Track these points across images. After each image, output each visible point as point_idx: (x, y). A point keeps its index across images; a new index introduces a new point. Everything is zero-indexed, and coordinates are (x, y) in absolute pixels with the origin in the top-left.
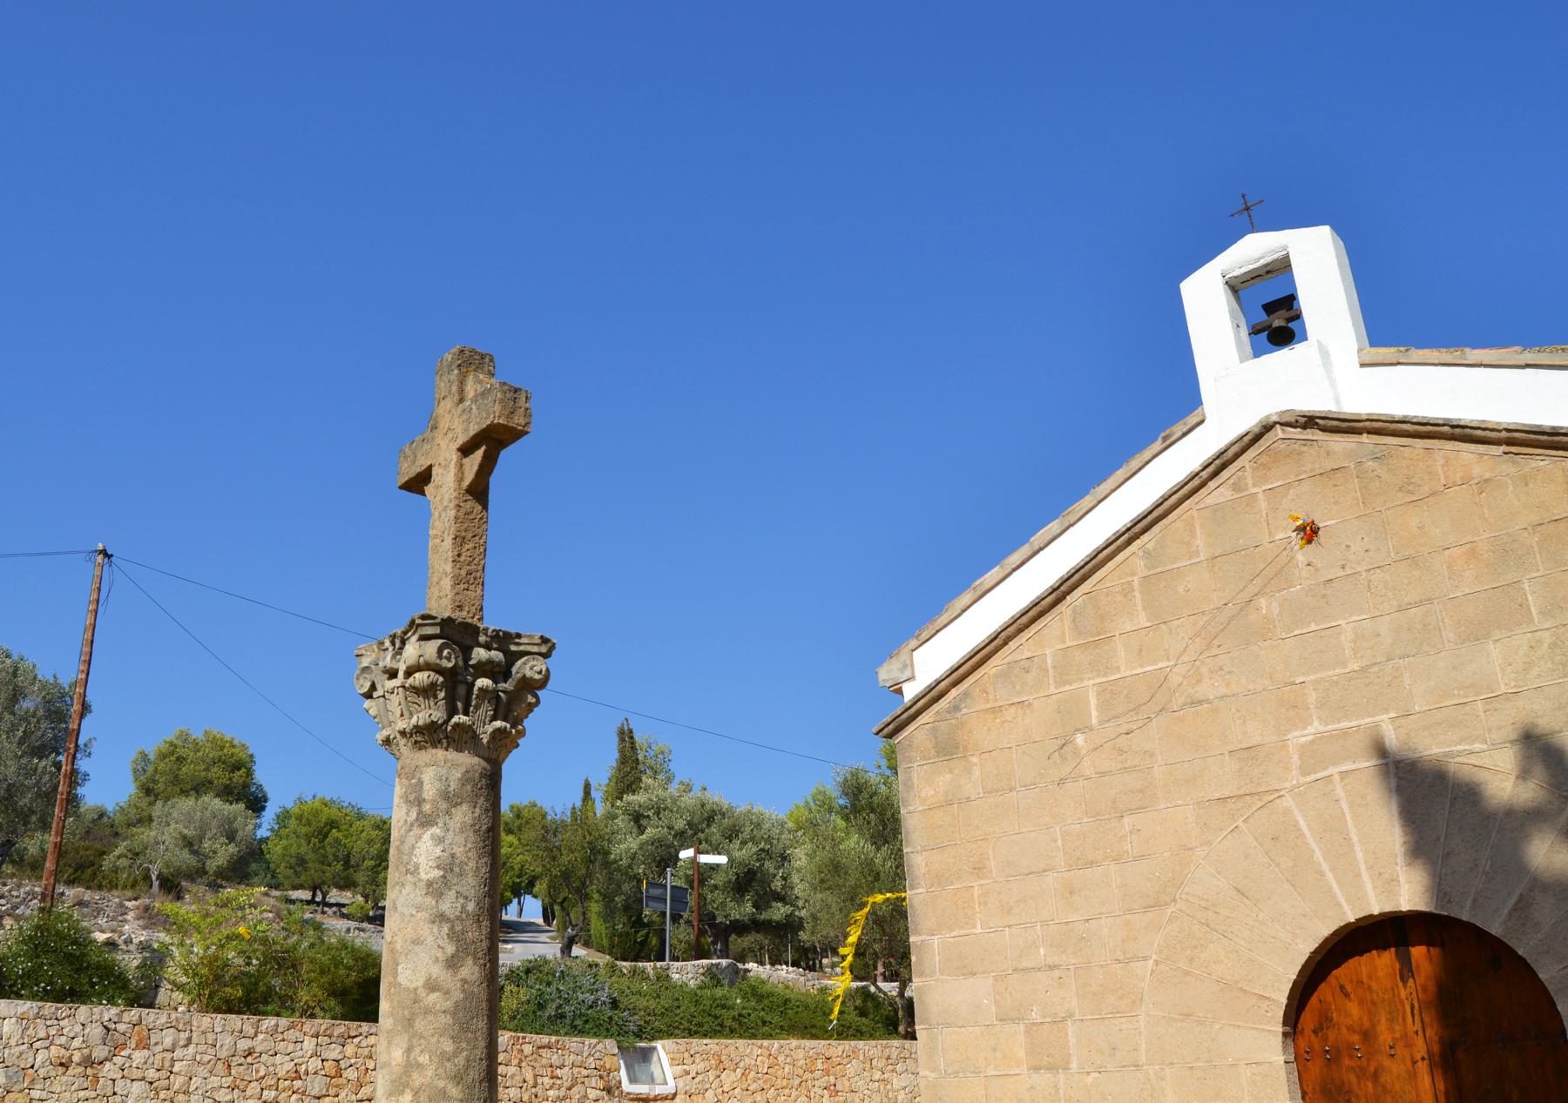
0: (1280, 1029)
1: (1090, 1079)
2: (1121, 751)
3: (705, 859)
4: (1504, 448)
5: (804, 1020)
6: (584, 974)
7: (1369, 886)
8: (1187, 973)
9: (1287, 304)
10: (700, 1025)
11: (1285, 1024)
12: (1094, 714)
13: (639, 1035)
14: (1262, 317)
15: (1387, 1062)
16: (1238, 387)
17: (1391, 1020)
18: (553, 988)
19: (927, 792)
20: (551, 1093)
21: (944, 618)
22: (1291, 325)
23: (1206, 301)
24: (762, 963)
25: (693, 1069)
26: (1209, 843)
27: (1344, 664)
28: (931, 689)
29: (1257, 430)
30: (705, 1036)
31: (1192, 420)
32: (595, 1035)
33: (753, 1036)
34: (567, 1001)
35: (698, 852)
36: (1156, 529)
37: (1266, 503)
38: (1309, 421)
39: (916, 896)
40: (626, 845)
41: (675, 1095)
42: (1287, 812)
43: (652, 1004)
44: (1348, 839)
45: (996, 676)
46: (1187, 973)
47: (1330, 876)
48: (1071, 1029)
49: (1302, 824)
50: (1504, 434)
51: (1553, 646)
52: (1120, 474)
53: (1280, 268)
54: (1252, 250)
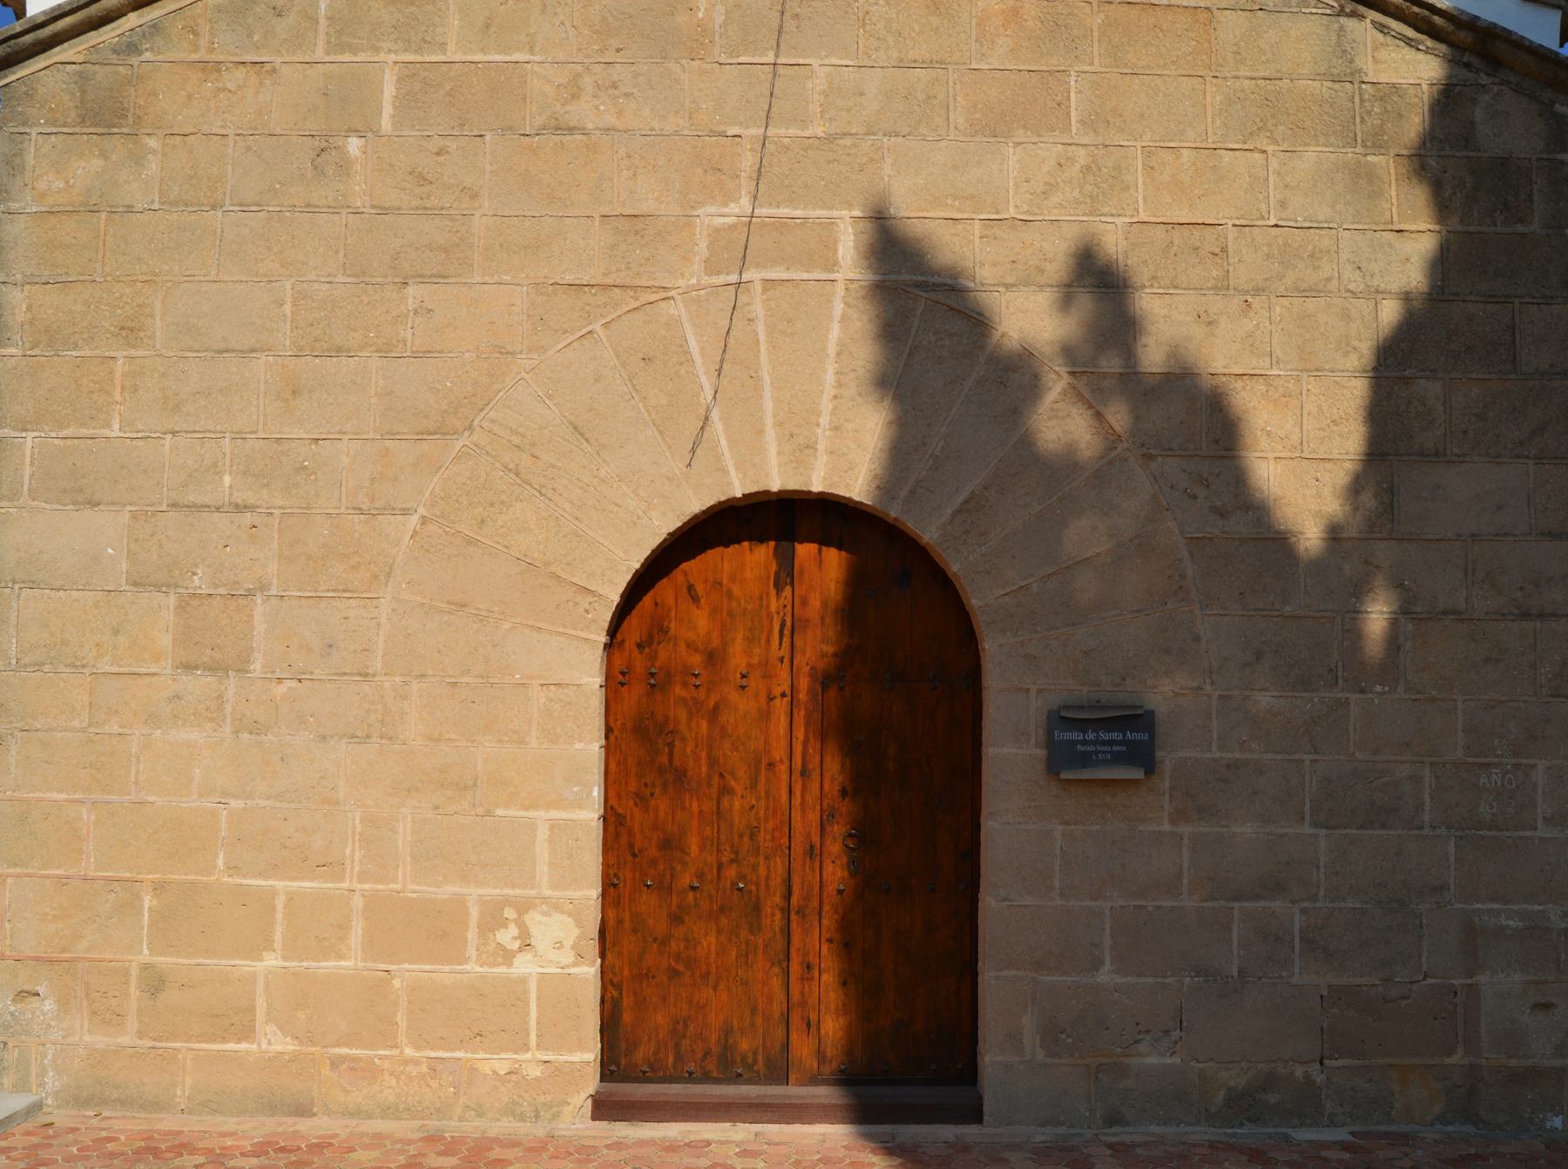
2: (423, 180)
7: (772, 449)
8: (471, 542)
12: (388, 109)
15: (734, 696)
17: (751, 639)
19: (51, 182)
26: (543, 349)
27: (804, 123)
44: (755, 379)
48: (260, 609)
51: (1087, 169)
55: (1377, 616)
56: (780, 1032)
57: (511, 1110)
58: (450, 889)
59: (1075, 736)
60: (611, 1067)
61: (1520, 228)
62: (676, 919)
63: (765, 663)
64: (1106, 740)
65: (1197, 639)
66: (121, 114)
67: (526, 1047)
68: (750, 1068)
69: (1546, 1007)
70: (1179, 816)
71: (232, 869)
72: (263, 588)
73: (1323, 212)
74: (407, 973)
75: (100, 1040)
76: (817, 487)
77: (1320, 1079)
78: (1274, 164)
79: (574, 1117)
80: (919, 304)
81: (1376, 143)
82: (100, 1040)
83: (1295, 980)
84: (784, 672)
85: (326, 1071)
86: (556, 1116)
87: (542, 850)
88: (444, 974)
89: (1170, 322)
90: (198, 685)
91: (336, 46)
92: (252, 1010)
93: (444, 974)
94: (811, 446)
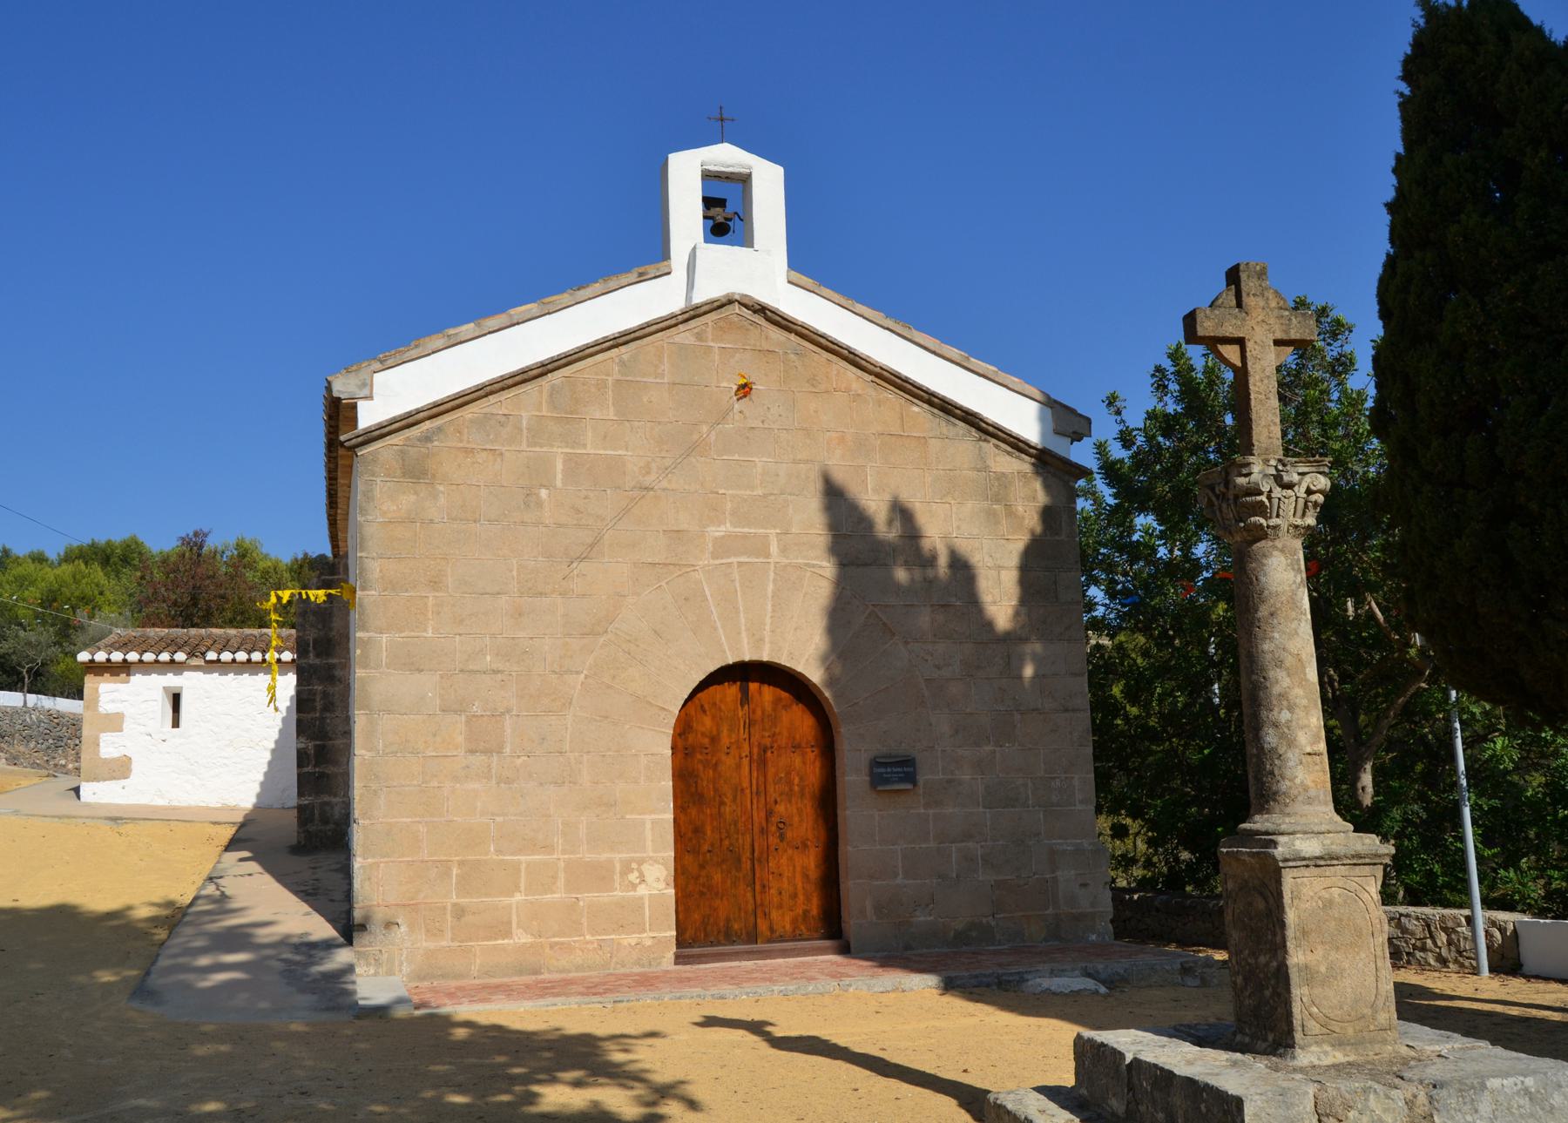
2: (578, 511)
4: (872, 378)
8: (609, 687)
12: (559, 476)
15: (724, 757)
17: (731, 730)
21: (414, 353)
23: (685, 174)
37: (725, 358)
38: (762, 310)
45: (471, 421)
48: (508, 722)
54: (726, 156)
58: (605, 856)
59: (882, 770)
60: (680, 943)
62: (702, 867)
63: (737, 741)
64: (895, 772)
66: (424, 473)
67: (644, 931)
69: (1084, 885)
70: (927, 806)
71: (499, 852)
72: (509, 711)
74: (587, 897)
75: (431, 945)
76: (765, 659)
77: (993, 924)
84: (746, 746)
85: (547, 950)
87: (648, 834)
88: (604, 897)
90: (478, 760)
92: (510, 923)
93: (604, 897)
94: (762, 639)
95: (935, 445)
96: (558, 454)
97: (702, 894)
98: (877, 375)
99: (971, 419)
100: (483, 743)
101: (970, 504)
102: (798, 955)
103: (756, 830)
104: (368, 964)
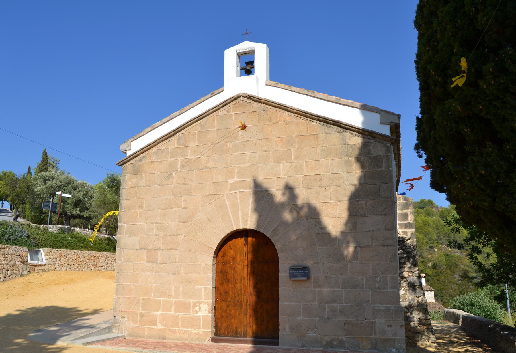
0: (213, 256)
1: (162, 266)
2: (185, 179)
3: (64, 195)
4: (295, 114)
5: (83, 244)
6: (19, 227)
7: (241, 221)
8: (192, 240)
9: (251, 63)
10: (56, 244)
11: (214, 254)
13: (35, 246)
14: (245, 65)
15: (237, 266)
16: (234, 84)
18: (8, 230)
19: (129, 183)
20: (3, 262)
21: (142, 134)
22: (252, 69)
23: (230, 56)
24: (81, 228)
25: (52, 257)
26: (203, 206)
27: (245, 163)
28: (135, 153)
29: (236, 97)
30: (57, 248)
31: (220, 90)
32: (21, 245)
33: (73, 249)
34: (12, 235)
35: (62, 193)
36: (205, 119)
37: (235, 116)
38: (250, 97)
39: (122, 213)
40: (39, 188)
41: (45, 265)
42: (224, 200)
43: (41, 237)
44: (238, 209)
45: (154, 153)
46: (192, 240)
47: (232, 218)
49: (227, 204)
50: (295, 111)
51: (295, 167)
52: (198, 101)
53: (251, 53)
54: (245, 46)
55: (351, 249)
56: (246, 328)
57: (197, 340)
58: (188, 300)
59: (294, 272)
61: (380, 169)
62: (228, 307)
63: (243, 260)
64: (301, 272)
65: (317, 253)
68: (240, 335)
69: (391, 326)
70: (315, 287)
71: (154, 296)
72: (160, 248)
73: (340, 170)
74: (181, 314)
75: (133, 325)
77: (344, 339)
78: (330, 162)
79: (208, 341)
80: (261, 195)
81: (350, 156)
82: (133, 325)
83: (339, 319)
86: (205, 341)
88: (187, 315)
89: (303, 196)
90: (150, 265)
91: (171, 157)
93: (187, 315)
94: (247, 220)
95: (322, 137)
96: (179, 159)
97: (227, 317)
98: (296, 113)
99: (337, 124)
100: (152, 260)
101: (338, 159)
102: (232, 343)
103: (249, 294)
104: (116, 329)
